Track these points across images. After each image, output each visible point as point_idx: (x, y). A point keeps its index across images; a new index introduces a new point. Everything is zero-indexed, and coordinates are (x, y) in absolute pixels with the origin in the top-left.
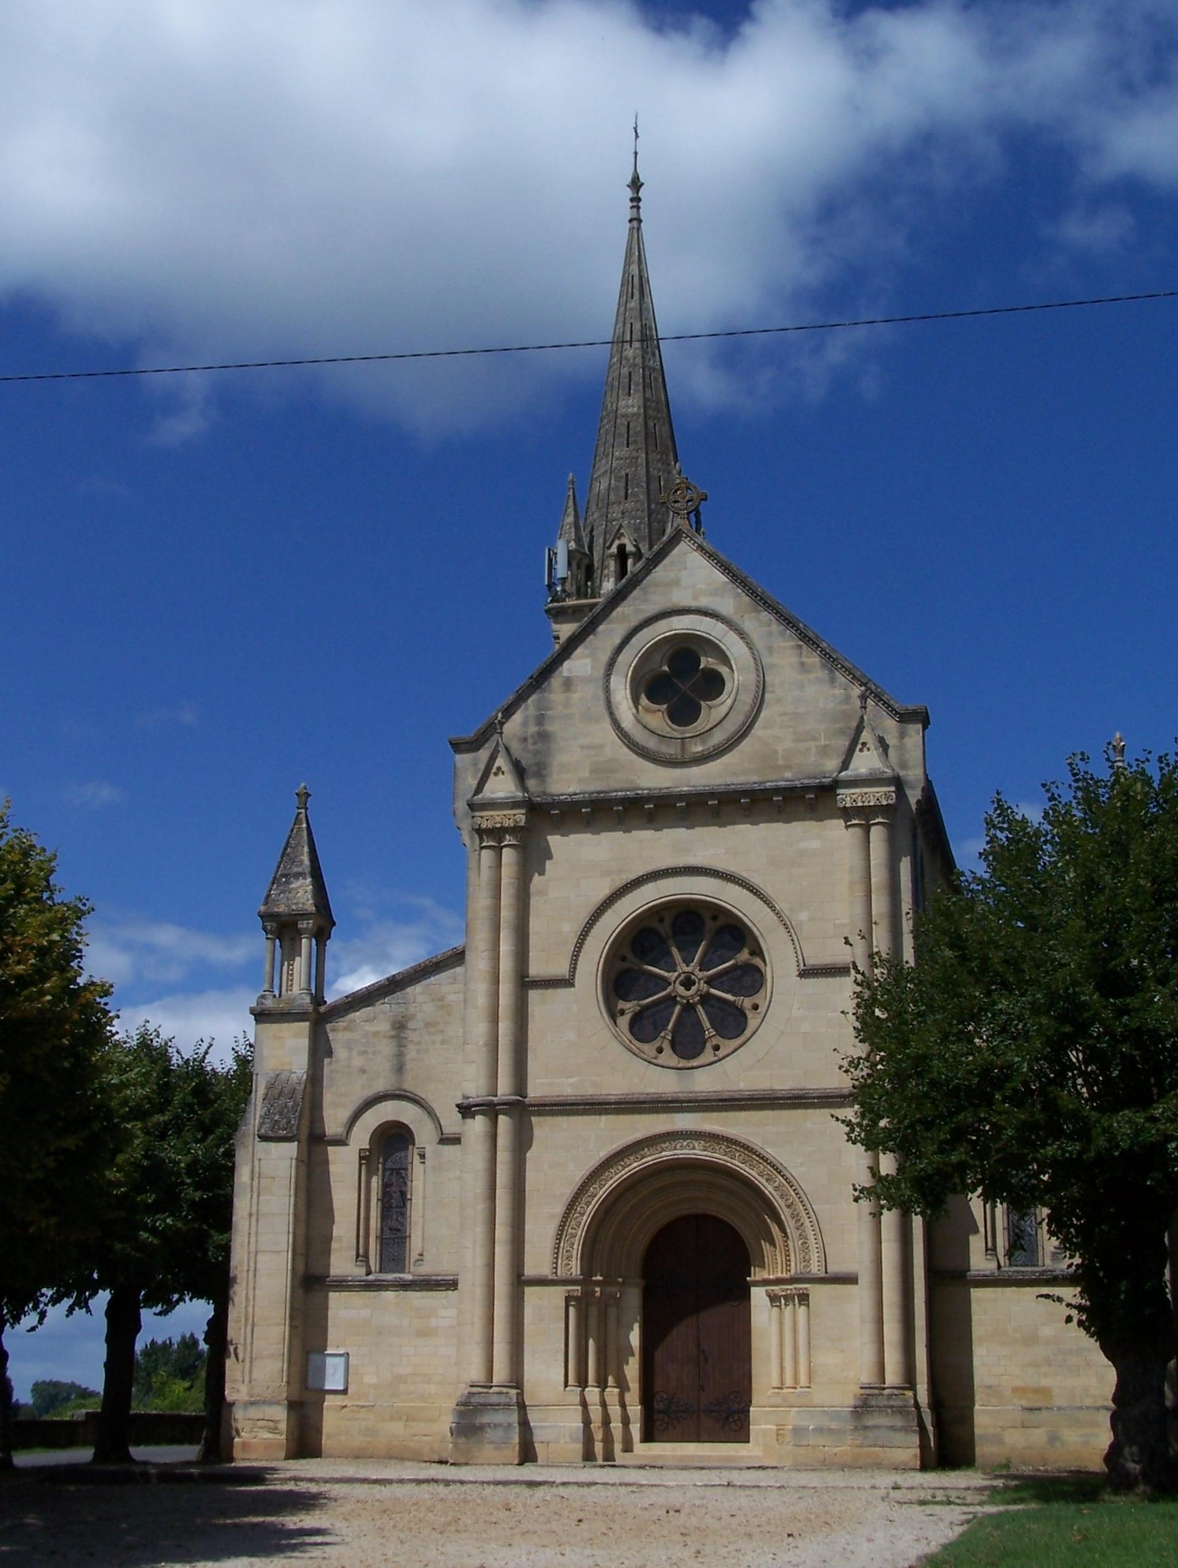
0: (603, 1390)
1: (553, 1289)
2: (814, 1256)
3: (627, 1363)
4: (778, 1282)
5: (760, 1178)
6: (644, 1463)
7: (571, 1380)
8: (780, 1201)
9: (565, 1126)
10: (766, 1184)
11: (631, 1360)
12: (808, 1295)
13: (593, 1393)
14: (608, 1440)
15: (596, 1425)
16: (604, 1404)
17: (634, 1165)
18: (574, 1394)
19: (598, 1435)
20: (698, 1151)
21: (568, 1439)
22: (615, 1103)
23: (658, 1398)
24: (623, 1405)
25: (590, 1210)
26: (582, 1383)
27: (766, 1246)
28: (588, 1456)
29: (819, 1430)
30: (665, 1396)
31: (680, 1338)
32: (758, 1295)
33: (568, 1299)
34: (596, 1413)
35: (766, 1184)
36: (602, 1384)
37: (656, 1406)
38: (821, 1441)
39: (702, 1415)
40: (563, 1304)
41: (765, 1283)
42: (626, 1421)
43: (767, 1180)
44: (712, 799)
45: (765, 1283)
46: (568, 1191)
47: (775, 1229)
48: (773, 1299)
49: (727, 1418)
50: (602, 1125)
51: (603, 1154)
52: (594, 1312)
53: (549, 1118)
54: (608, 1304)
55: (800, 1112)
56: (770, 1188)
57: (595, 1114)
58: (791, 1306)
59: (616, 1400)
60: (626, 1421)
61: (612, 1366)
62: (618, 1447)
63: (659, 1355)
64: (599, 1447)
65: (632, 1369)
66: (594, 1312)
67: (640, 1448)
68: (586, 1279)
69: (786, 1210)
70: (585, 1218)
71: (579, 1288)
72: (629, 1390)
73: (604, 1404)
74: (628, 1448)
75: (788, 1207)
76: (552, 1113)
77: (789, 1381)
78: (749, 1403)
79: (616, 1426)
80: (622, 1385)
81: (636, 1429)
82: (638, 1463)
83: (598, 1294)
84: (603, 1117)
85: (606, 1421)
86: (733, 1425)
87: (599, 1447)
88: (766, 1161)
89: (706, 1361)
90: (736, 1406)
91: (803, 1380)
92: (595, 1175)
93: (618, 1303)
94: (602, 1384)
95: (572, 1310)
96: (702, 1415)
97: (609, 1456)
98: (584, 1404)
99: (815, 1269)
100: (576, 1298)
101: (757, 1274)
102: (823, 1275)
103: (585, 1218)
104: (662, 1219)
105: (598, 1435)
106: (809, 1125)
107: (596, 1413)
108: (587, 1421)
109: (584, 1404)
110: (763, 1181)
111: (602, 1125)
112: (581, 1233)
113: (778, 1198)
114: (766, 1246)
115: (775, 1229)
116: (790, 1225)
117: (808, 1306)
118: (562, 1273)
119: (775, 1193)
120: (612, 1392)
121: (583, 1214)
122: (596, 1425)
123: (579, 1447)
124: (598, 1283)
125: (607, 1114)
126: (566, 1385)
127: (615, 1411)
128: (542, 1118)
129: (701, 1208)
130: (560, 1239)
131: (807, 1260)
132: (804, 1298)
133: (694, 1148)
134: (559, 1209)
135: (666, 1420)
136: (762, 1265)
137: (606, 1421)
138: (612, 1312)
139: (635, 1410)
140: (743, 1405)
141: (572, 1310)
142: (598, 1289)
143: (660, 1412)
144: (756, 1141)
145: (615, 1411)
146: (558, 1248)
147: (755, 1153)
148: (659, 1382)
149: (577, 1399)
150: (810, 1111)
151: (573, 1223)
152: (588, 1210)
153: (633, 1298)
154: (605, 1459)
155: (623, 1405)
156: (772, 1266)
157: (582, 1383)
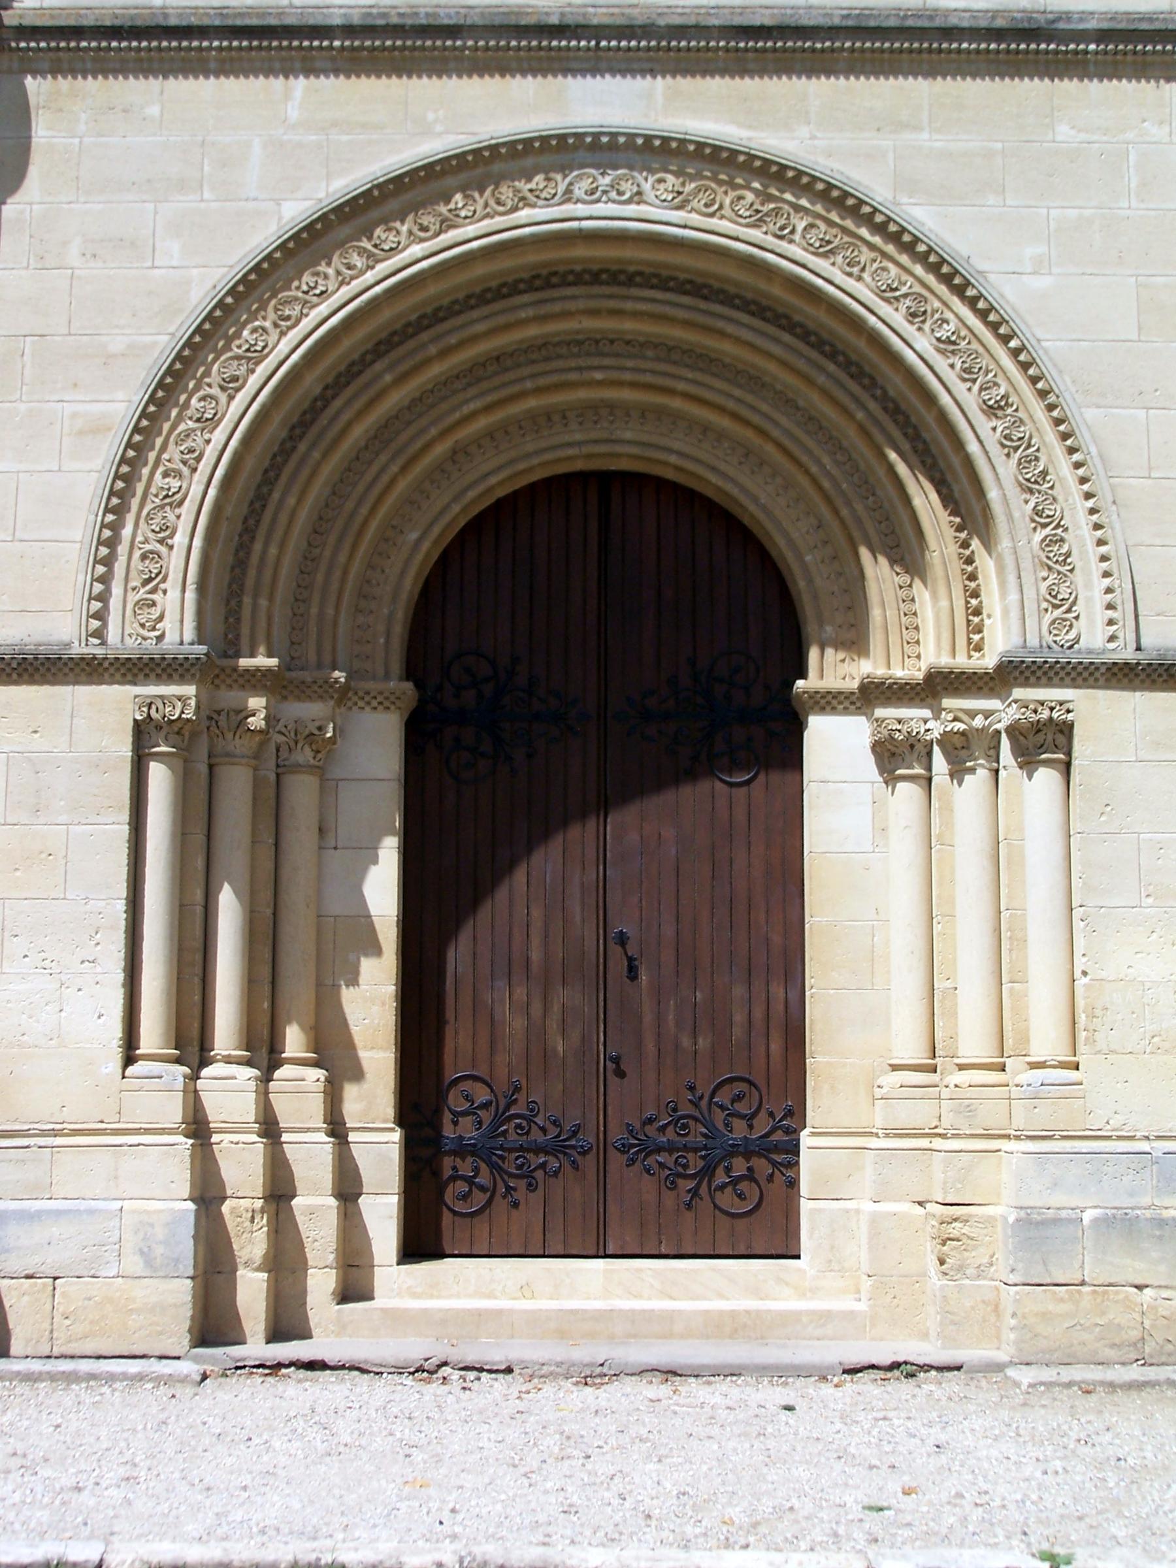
0: (267, 1078)
1: (85, 693)
2: (1090, 589)
3: (354, 981)
4: (937, 686)
5: (885, 309)
6: (439, 1352)
7: (151, 1036)
8: (960, 388)
9: (154, 110)
10: (909, 330)
11: (367, 965)
12: (1066, 730)
13: (229, 1090)
14: (286, 1260)
15: (243, 1206)
16: (269, 1128)
17: (411, 251)
18: (159, 1090)
19: (251, 1243)
20: (651, 207)
21: (133, 1263)
22: (349, 30)
23: (456, 1101)
24: (337, 1129)
25: (238, 411)
26: (192, 1046)
27: (879, 573)
28: (213, 1326)
29: (1121, 1225)
30: (482, 1095)
31: (540, 895)
32: (835, 747)
33: (143, 733)
34: (241, 1165)
35: (909, 330)
36: (264, 1053)
37: (448, 1131)
38: (1132, 1266)
39: (616, 1160)
40: (125, 750)
41: (870, 695)
42: (348, 1188)
43: (912, 315)
44: (235, 332)
45: (870, 695)
46: (161, 342)
47: (925, 500)
48: (894, 756)
49: (708, 1172)
50: (293, 112)
51: (296, 210)
52: (237, 786)
53: (92, 85)
54: (284, 761)
55: (1030, 90)
56: (924, 343)
57: (269, 71)
58: (978, 780)
59: (314, 1108)
60: (348, 1188)
61: (298, 990)
62: (321, 1282)
63: (459, 956)
64: (251, 1291)
65: (371, 1003)
66: (237, 786)
67: (397, 1283)
68: (214, 667)
69: (984, 425)
70: (219, 436)
71: (190, 690)
72: (358, 1074)
73: (269, 1128)
74: (354, 1289)
75: (992, 410)
76: (103, 67)
77: (972, 1039)
78: (796, 1114)
79: (315, 1206)
80: (335, 1057)
81: (382, 1215)
82: (415, 1349)
83: (256, 722)
84: (300, 85)
85: (279, 1191)
86: (726, 1199)
87: (251, 1291)
88: (909, 248)
89: (632, 972)
90: (740, 1129)
91: (1046, 1040)
92: (263, 282)
93: (323, 751)
94: (264, 1053)
95: (159, 777)
96: (616, 1160)
97: (286, 1323)
98: (198, 1127)
99: (1093, 637)
100: (176, 729)
101: (828, 670)
102: (1129, 655)
103: (219, 436)
104: (495, 476)
105: (251, 1243)
106: (1064, 131)
107: (241, 1165)
108: (208, 1194)
109: (198, 1127)
110: (898, 318)
111: (293, 112)
112: (200, 490)
113: (951, 377)
114: (879, 573)
115: (925, 500)
116: (1000, 479)
117: (1066, 768)
118: (123, 636)
119: (941, 364)
120: (299, 1087)
121: (212, 423)
122: (243, 1206)
123: (178, 1294)
124: (256, 680)
125: (310, 70)
126: (129, 1059)
127: (311, 1156)
128: (64, 84)
129: (627, 447)
130: (119, 511)
131: (1061, 604)
132: (1046, 742)
133: (638, 197)
134: (123, 403)
135: (484, 1179)
136: (855, 641)
137: (279, 1191)
138: (302, 792)
139: (381, 1151)
140: (762, 1125)
141: (159, 777)
142: (256, 703)
143: (462, 1150)
144: (874, 185)
145: (311, 1156)
146: (112, 543)
147: (868, 220)
148: (460, 1045)
149: (173, 1111)
150: (1069, 87)
151: (173, 452)
152: (230, 413)
153: (375, 748)
154: (276, 1335)
155: (337, 1129)
156: (913, 623)
157: (192, 1046)
